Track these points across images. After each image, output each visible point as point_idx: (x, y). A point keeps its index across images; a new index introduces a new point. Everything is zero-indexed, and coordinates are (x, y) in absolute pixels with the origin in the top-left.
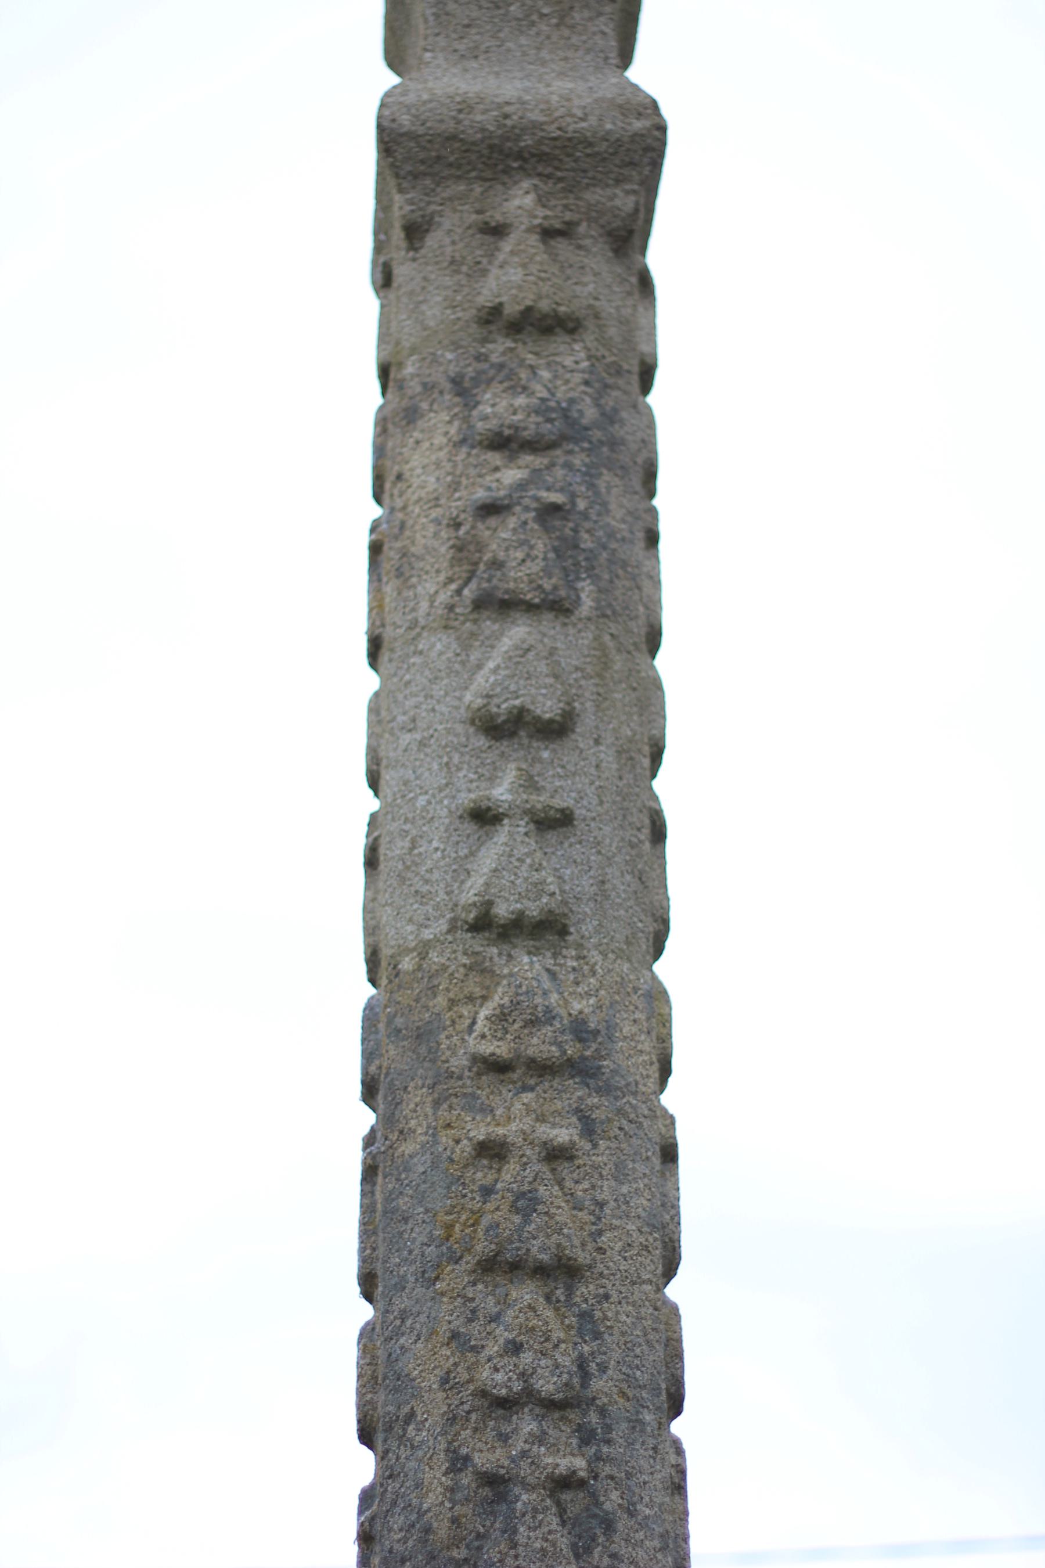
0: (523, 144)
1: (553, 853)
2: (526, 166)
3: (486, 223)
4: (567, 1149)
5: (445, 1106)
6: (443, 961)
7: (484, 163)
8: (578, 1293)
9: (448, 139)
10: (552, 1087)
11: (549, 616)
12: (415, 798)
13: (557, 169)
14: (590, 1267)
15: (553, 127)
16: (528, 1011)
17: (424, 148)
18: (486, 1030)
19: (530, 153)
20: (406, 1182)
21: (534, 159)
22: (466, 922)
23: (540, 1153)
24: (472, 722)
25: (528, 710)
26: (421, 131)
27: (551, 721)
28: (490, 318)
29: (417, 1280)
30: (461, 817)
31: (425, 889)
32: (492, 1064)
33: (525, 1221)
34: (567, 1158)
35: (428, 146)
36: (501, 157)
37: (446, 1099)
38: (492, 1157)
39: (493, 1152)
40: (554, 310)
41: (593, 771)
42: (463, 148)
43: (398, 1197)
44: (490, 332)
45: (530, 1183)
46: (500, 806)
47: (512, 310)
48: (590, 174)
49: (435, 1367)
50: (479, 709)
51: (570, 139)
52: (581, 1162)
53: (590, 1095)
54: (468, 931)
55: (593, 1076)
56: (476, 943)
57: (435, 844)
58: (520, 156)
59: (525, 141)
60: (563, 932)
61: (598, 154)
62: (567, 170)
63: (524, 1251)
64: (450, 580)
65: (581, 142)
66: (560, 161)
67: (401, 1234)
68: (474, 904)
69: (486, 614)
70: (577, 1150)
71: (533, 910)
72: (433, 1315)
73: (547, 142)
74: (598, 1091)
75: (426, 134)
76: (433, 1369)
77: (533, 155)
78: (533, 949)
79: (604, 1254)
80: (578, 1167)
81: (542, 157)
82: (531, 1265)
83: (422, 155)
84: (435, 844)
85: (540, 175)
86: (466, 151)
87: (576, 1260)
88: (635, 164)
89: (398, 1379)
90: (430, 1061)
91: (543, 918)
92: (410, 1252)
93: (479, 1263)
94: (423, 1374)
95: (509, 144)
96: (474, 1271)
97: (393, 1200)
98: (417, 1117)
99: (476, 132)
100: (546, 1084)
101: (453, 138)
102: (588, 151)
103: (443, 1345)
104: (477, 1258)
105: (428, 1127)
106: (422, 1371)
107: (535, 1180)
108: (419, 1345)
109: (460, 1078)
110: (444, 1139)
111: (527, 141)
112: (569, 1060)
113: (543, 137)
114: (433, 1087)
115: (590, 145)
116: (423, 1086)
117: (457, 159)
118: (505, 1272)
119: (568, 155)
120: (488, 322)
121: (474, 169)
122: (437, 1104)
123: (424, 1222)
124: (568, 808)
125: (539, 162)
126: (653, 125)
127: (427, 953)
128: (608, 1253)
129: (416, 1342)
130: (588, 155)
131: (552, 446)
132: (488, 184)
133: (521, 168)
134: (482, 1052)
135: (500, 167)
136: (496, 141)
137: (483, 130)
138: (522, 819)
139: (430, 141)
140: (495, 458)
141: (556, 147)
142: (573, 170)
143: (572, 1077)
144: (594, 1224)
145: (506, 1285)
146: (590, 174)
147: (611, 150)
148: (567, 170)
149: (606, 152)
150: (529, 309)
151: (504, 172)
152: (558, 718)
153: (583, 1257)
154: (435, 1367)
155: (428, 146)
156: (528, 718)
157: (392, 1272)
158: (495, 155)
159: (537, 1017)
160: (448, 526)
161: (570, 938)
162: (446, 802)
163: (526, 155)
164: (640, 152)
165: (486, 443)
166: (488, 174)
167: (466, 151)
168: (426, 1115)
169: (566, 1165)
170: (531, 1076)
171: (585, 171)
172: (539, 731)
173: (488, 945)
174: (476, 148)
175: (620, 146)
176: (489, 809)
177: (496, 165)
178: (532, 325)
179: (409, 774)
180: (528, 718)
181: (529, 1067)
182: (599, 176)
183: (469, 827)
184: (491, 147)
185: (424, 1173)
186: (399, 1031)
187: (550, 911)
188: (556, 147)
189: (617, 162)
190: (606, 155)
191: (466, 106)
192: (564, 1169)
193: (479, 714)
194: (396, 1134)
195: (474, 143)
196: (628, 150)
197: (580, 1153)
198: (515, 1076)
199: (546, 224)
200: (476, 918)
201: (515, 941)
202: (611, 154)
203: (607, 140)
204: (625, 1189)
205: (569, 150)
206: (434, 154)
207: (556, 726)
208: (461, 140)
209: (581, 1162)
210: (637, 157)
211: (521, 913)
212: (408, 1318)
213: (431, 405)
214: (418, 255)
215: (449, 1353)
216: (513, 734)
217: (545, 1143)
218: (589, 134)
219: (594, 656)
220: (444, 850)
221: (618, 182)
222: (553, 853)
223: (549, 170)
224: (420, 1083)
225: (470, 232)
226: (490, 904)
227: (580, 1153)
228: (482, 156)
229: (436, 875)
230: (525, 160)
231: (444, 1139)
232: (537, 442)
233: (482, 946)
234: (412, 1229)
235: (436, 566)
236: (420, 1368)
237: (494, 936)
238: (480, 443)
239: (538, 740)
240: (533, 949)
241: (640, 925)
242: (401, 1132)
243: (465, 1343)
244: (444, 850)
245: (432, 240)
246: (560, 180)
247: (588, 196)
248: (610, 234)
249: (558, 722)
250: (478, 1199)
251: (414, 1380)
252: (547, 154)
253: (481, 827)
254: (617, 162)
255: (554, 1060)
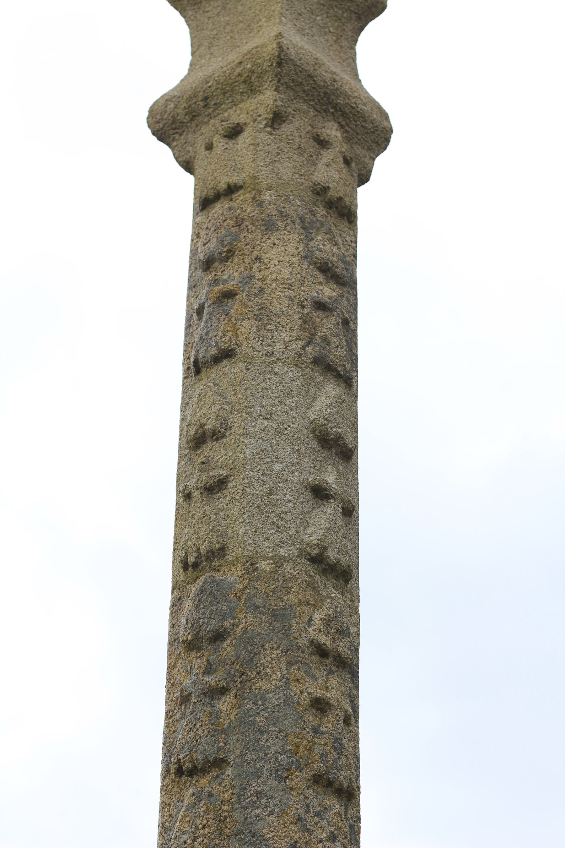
0: (339, 101)
2: (335, 114)
3: (318, 135)
5: (296, 667)
6: (295, 573)
7: (319, 100)
10: (341, 676)
12: (272, 463)
15: (353, 100)
16: (340, 624)
18: (321, 627)
19: (340, 108)
20: (262, 707)
21: (341, 113)
22: (310, 555)
24: (313, 431)
25: (343, 438)
26: (298, 63)
29: (271, 774)
30: (305, 487)
31: (281, 523)
32: (322, 650)
36: (327, 102)
37: (296, 663)
38: (318, 709)
39: (320, 706)
42: (313, 86)
43: (255, 715)
46: (332, 490)
47: (333, 194)
48: (359, 137)
49: (286, 836)
50: (322, 426)
51: (358, 112)
54: (308, 560)
56: (311, 569)
57: (288, 497)
59: (340, 100)
61: (366, 128)
62: (351, 128)
64: (298, 338)
65: (362, 117)
67: (257, 741)
68: (318, 545)
69: (317, 368)
72: (284, 801)
73: (349, 107)
75: (300, 67)
76: (284, 837)
77: (341, 111)
82: (337, 786)
83: (295, 77)
84: (288, 497)
85: (339, 123)
86: (314, 88)
89: (253, 837)
90: (284, 634)
92: (266, 755)
93: (314, 776)
94: (276, 838)
96: (309, 780)
97: (251, 716)
98: (272, 667)
99: (321, 81)
102: (363, 124)
103: (292, 823)
104: (314, 772)
105: (283, 677)
106: (275, 836)
108: (272, 818)
109: (303, 652)
110: (295, 688)
111: (340, 101)
113: (348, 103)
114: (286, 652)
116: (278, 649)
117: (308, 90)
118: (324, 786)
120: (318, 194)
121: (313, 100)
122: (289, 663)
123: (277, 737)
125: (342, 115)
127: (282, 564)
129: (269, 815)
130: (362, 126)
132: (316, 113)
133: (333, 113)
134: (319, 640)
135: (324, 107)
136: (329, 92)
137: (325, 81)
138: (340, 504)
139: (301, 72)
140: (321, 277)
145: (322, 794)
146: (359, 137)
148: (351, 128)
149: (369, 129)
154: (286, 836)
156: (341, 443)
157: (249, 763)
158: (325, 99)
159: (343, 629)
160: (298, 304)
162: (296, 474)
164: (383, 139)
165: (318, 265)
166: (318, 107)
168: (280, 669)
171: (357, 134)
172: (342, 453)
173: (316, 573)
175: (377, 130)
176: (326, 489)
179: (266, 446)
180: (341, 443)
181: (335, 659)
183: (309, 495)
184: (325, 93)
185: (277, 705)
186: (258, 607)
187: (182, 561)
190: (369, 131)
191: (317, 63)
193: (320, 428)
194: (255, 673)
195: (319, 86)
200: (317, 554)
201: (329, 577)
202: (371, 132)
203: (373, 124)
205: (356, 118)
208: (314, 81)
212: (263, 798)
213: (286, 226)
214: (274, 133)
215: (296, 829)
220: (295, 503)
223: (343, 123)
224: (275, 646)
225: (308, 136)
226: (326, 548)
228: (320, 95)
229: (289, 517)
230: (336, 110)
231: (295, 688)
232: (340, 278)
233: (314, 572)
234: (267, 740)
235: (290, 325)
236: (273, 834)
237: (320, 569)
238: (315, 264)
239: (339, 458)
242: (258, 673)
243: (304, 826)
244: (295, 503)
245: (286, 129)
246: (347, 132)
250: (311, 733)
251: (267, 840)
252: (347, 114)
253: (314, 498)
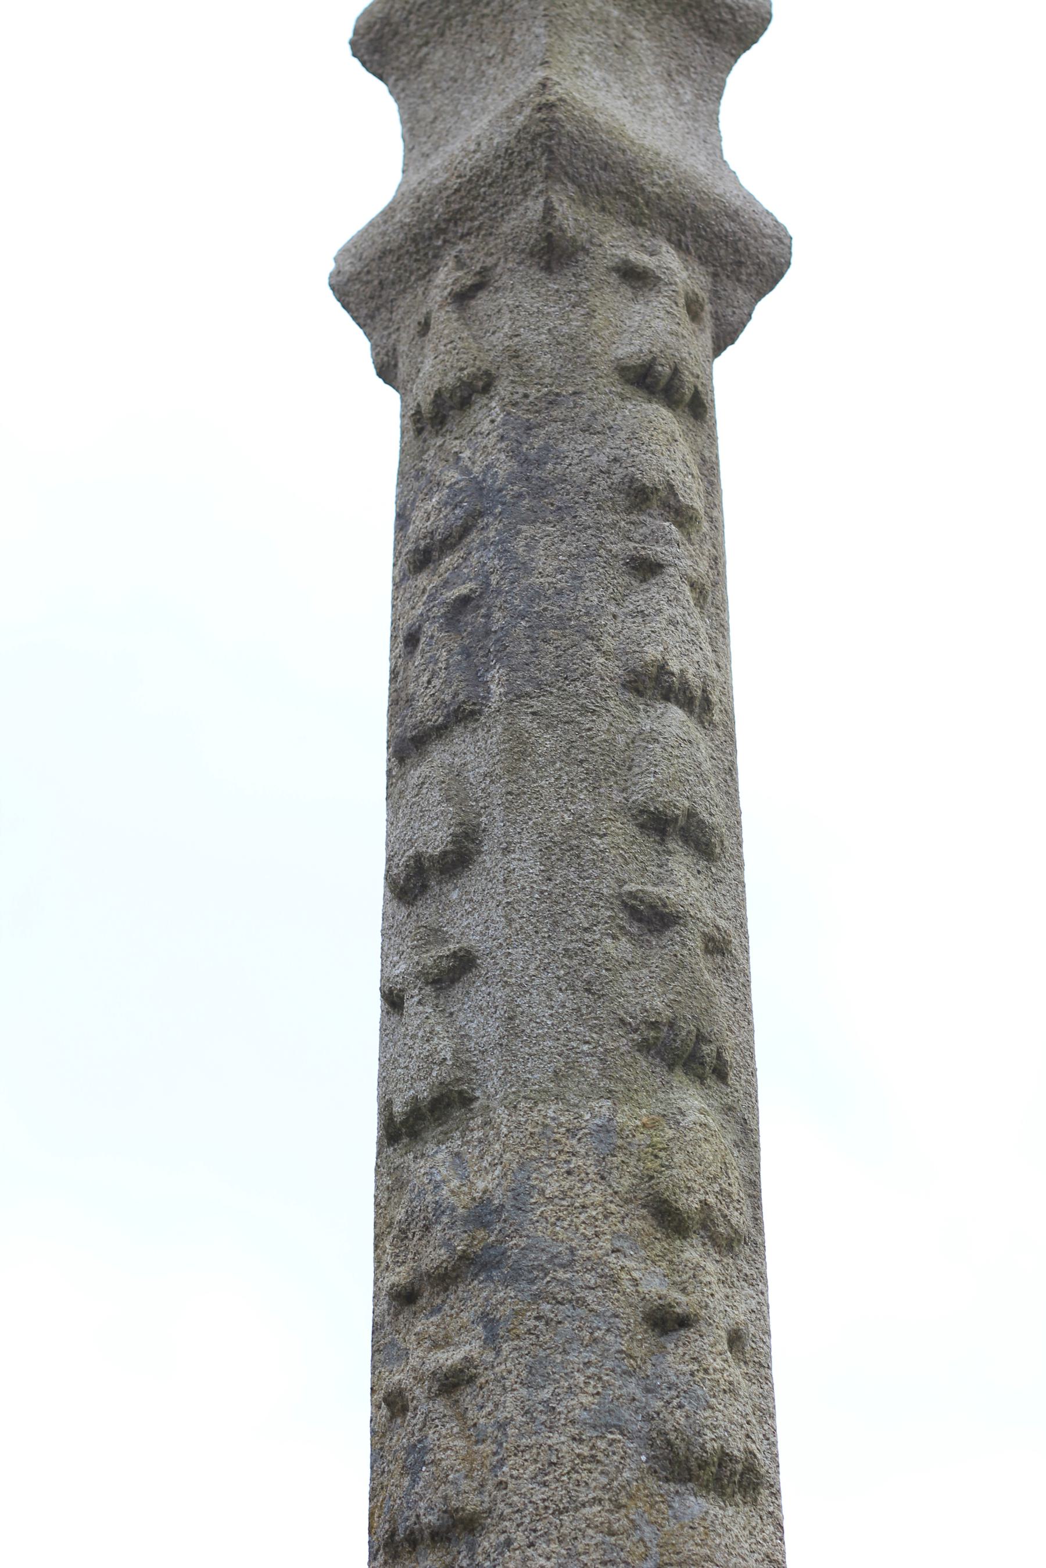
1: (460, 1010)
4: (461, 1371)
7: (416, 260)
8: (480, 1550)
9: (380, 258)
11: (458, 730)
13: (472, 219)
14: (490, 1511)
17: (368, 282)
19: (445, 220)
23: (430, 1388)
27: (444, 854)
28: (419, 425)
33: (414, 1481)
34: (468, 1382)
35: (369, 277)
40: (460, 379)
41: (501, 889)
44: (425, 441)
45: (420, 1430)
51: (470, 181)
52: (482, 1380)
53: (495, 1291)
55: (498, 1265)
58: (440, 231)
60: (466, 1100)
62: (481, 214)
63: (413, 1519)
65: (479, 177)
66: (472, 209)
70: (476, 1368)
71: (423, 1090)
74: (506, 1282)
78: (441, 1137)
79: (506, 1488)
80: (481, 1388)
81: (455, 218)
87: (463, 1509)
88: (533, 163)
91: (435, 1095)
95: (426, 226)
100: (452, 1297)
101: (384, 253)
107: (424, 1425)
112: (461, 1258)
115: (487, 172)
119: (475, 199)
121: (411, 273)
124: (661, 932)
126: (533, 110)
128: (510, 1486)
130: (490, 185)
131: (466, 530)
133: (445, 241)
136: (416, 230)
141: (462, 198)
142: (486, 209)
143: (476, 1276)
144: (495, 1454)
147: (506, 165)
150: (438, 394)
151: (435, 256)
152: (450, 847)
153: (473, 1503)
155: (369, 277)
158: (421, 245)
161: (476, 1105)
163: (443, 226)
167: (398, 259)
169: (469, 1390)
170: (438, 1294)
174: (403, 251)
177: (426, 255)
178: (452, 408)
182: (508, 199)
188: (462, 198)
189: (516, 173)
190: (504, 173)
192: (467, 1397)
195: (400, 247)
196: (520, 152)
197: (481, 1370)
198: (423, 1302)
199: (457, 288)
204: (545, 1394)
205: (474, 193)
206: (376, 282)
207: (450, 858)
209: (482, 1380)
210: (529, 154)
211: (415, 1098)
216: (424, 888)
217: (434, 1373)
218: (482, 163)
219: (504, 750)
221: (525, 192)
222: (460, 1010)
227: (481, 1370)
240: (441, 1137)
241: (585, 1047)
247: (505, 228)
248: (532, 255)
249: (452, 851)
252: (459, 210)
254: (516, 173)
255: (444, 1265)
